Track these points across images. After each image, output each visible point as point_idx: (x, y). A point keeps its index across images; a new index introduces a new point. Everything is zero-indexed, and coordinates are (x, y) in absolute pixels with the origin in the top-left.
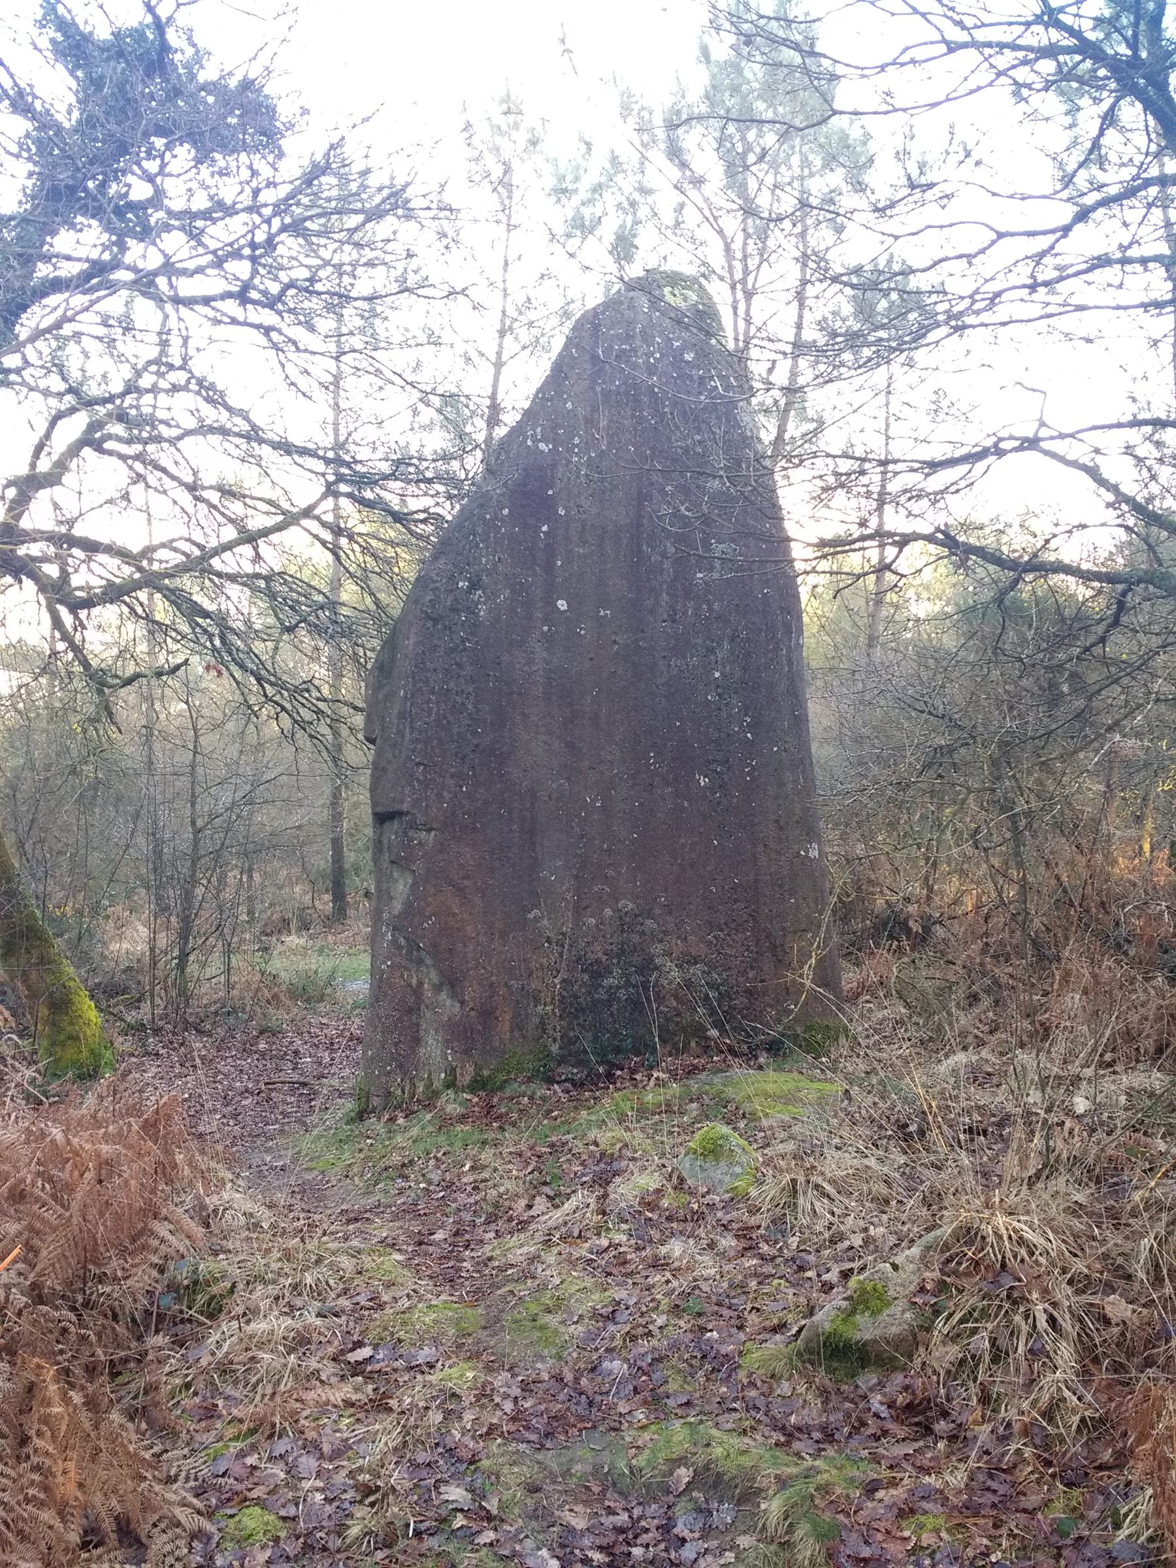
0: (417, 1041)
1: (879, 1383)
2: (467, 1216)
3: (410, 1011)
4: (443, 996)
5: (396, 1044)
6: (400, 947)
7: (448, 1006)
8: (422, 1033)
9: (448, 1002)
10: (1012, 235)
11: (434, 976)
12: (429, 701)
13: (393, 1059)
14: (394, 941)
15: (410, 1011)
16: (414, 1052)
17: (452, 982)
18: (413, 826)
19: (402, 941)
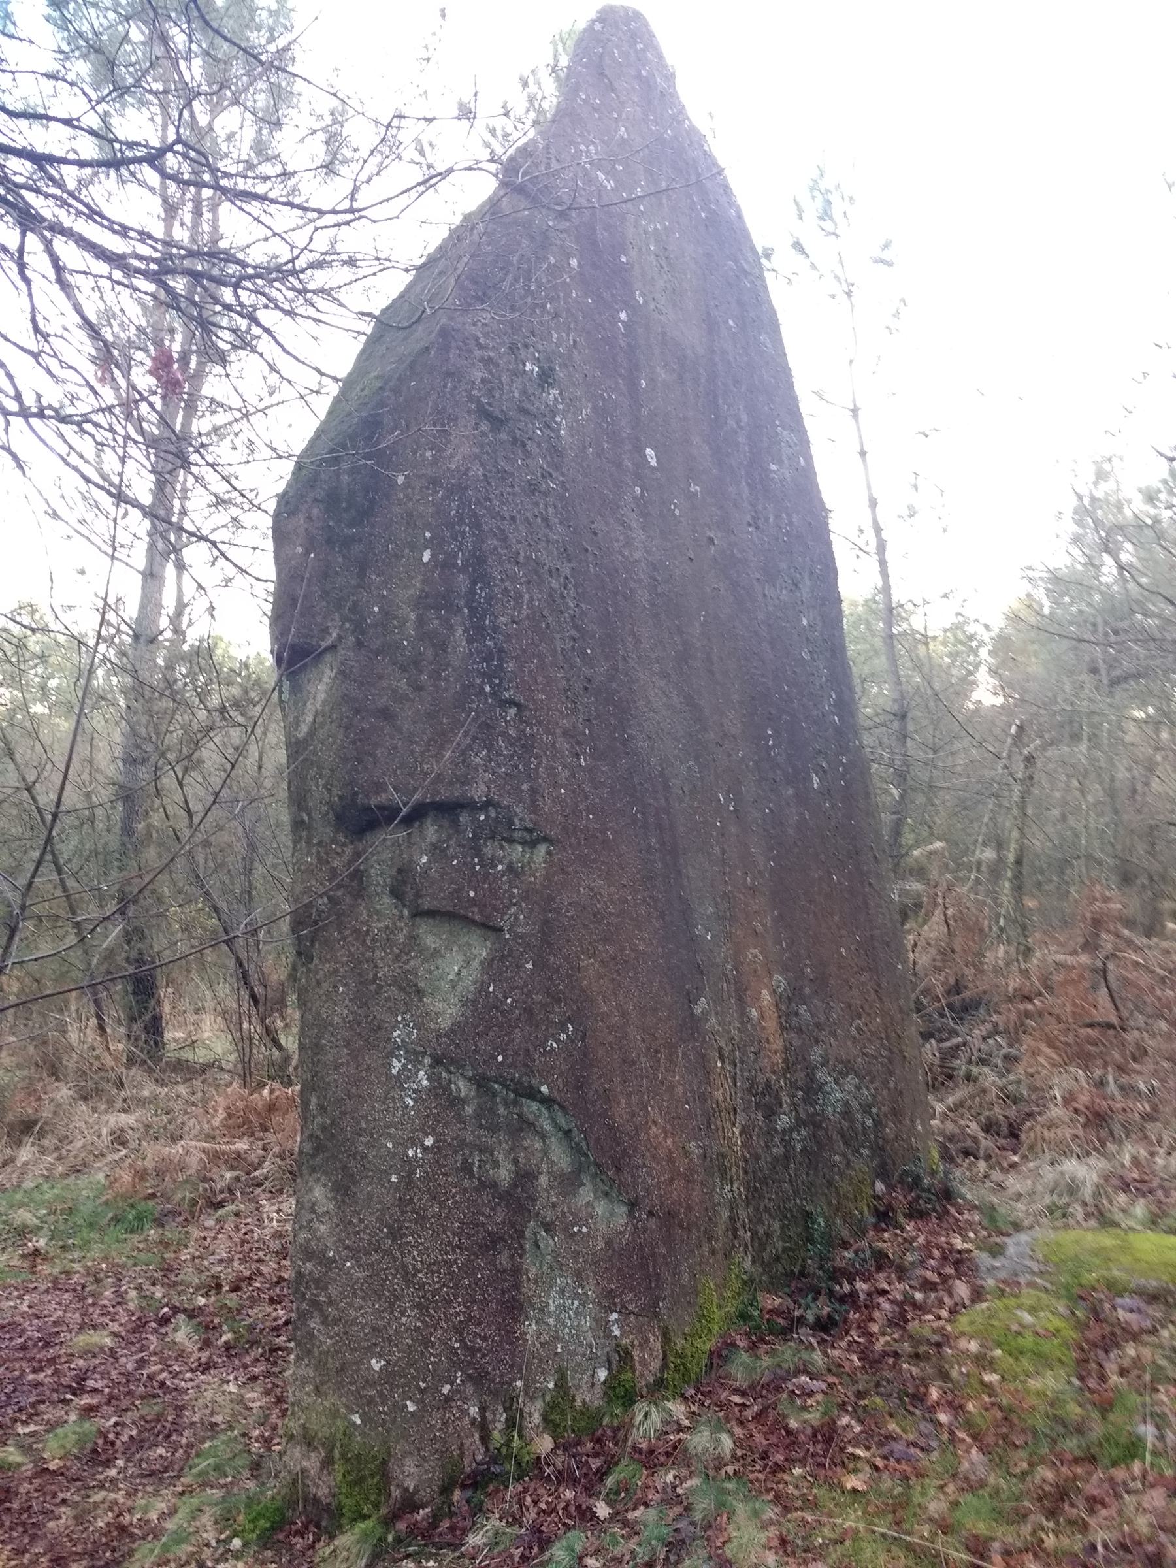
0: (514, 1308)
1: (629, 1398)
2: (30, 1343)
3: (493, 1242)
4: (586, 1194)
5: (459, 1329)
6: (455, 1102)
7: (602, 1214)
8: (528, 1288)
9: (600, 1208)
10: (15, 344)
11: (560, 1157)
12: (513, 578)
13: (455, 1364)
14: (440, 1090)
15: (493, 1242)
16: (510, 1336)
17: (607, 1157)
18: (503, 831)
19: (462, 1087)
